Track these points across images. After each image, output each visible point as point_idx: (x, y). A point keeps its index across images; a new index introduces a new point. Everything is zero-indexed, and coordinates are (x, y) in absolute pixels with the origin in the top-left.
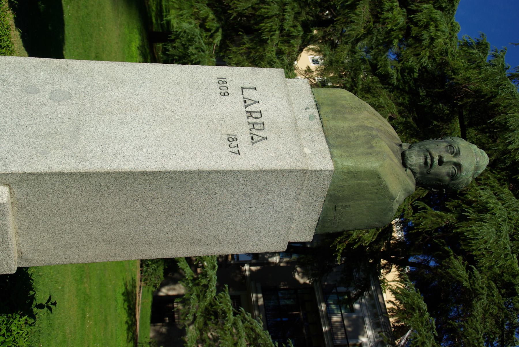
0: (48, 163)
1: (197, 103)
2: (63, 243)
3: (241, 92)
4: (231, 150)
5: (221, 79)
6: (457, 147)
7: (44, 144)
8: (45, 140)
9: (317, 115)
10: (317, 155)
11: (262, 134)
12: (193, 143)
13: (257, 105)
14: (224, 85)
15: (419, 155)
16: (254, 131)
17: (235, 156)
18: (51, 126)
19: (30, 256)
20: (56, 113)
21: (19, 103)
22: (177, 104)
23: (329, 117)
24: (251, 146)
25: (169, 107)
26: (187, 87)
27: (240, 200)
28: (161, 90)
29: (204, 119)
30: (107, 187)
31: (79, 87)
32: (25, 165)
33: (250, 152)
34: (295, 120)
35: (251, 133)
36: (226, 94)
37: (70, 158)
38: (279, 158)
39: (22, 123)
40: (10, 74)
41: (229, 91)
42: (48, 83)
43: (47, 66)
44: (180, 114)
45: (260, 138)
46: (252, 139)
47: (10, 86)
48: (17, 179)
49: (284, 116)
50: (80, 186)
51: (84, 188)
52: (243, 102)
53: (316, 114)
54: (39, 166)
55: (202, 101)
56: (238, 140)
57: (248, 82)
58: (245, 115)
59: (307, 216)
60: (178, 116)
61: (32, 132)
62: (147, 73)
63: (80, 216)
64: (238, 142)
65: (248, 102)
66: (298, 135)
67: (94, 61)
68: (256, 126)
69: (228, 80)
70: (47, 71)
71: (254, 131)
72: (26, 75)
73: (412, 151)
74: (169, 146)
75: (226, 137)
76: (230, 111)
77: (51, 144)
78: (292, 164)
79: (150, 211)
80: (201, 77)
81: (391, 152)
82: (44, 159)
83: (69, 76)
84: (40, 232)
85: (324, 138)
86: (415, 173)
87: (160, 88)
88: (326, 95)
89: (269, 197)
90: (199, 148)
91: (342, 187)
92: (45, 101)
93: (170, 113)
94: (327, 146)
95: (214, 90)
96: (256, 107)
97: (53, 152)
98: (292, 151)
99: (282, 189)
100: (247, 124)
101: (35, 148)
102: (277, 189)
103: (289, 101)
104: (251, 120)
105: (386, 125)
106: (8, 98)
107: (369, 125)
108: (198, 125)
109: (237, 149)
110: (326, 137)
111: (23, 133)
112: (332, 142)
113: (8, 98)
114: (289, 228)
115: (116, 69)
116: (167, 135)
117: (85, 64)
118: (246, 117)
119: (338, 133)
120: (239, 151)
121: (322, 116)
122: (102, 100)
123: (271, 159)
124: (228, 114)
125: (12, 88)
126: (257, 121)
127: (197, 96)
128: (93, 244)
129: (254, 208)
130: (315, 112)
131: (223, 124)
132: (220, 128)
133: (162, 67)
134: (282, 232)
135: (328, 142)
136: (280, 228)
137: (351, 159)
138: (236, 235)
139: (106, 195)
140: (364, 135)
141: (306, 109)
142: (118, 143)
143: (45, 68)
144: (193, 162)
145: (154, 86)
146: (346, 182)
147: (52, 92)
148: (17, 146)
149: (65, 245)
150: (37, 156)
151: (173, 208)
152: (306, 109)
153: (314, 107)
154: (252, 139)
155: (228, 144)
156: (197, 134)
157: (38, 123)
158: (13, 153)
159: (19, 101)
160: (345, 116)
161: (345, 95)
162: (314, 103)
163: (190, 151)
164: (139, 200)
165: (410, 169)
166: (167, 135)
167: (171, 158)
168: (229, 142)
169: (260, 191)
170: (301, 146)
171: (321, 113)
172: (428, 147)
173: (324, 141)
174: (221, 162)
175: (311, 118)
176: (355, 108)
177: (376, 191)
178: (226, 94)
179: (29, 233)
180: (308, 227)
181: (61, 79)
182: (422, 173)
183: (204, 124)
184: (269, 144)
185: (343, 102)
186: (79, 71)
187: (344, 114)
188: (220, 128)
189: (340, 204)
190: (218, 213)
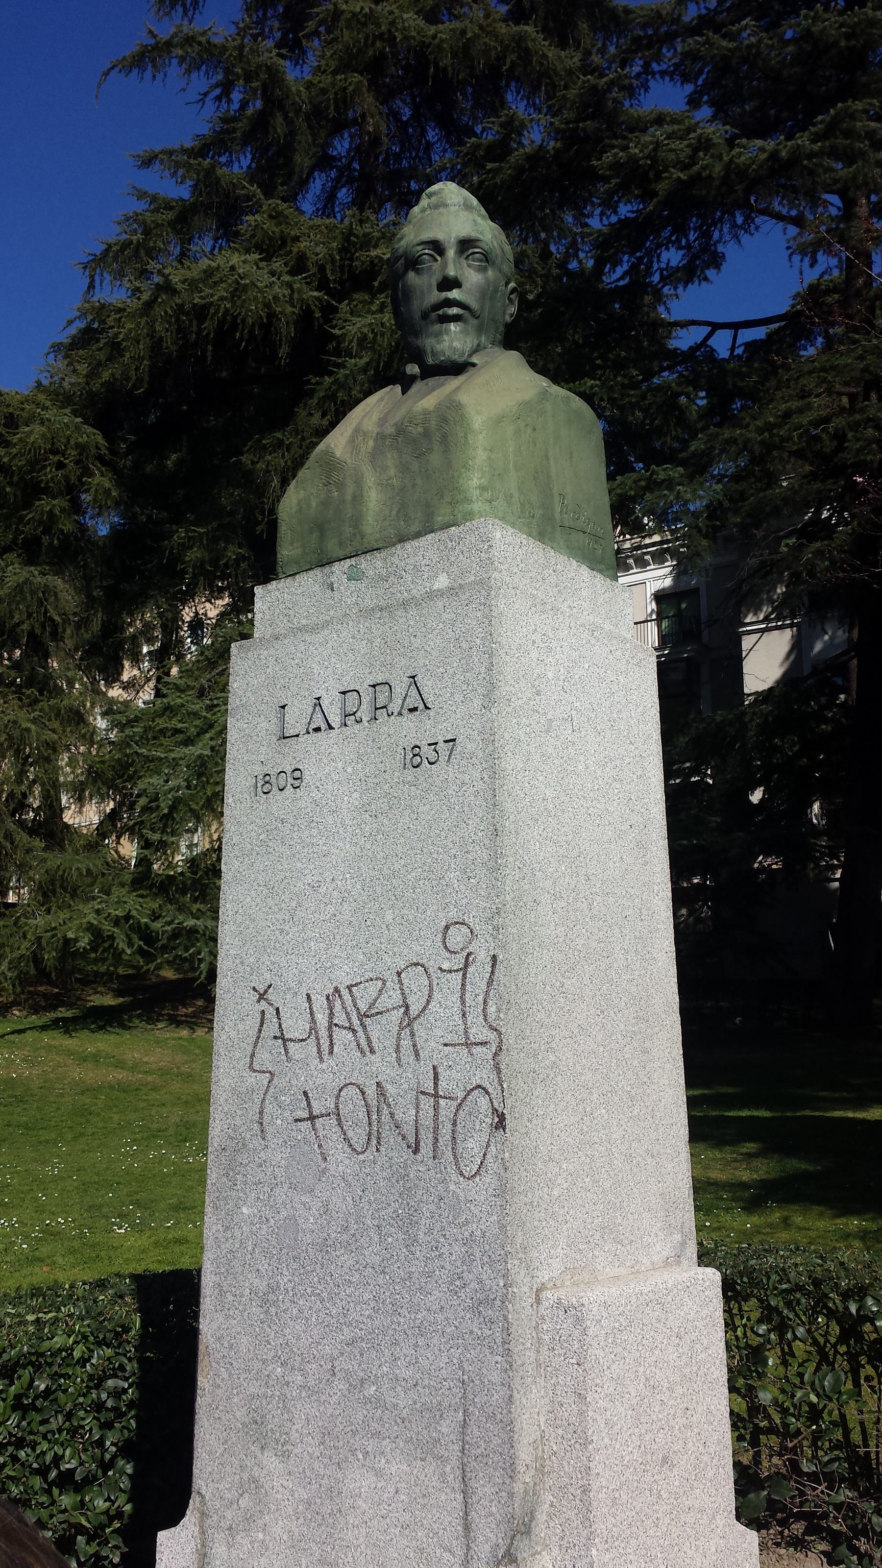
0: (482, 1198)
1: (321, 842)
2: (649, 1160)
3: (293, 741)
4: (443, 758)
5: (259, 789)
6: (419, 248)
7: (432, 1207)
8: (422, 1205)
9: (348, 562)
10: (453, 559)
11: (399, 690)
12: (425, 850)
13: (325, 703)
14: (273, 780)
15: (438, 335)
16: (395, 707)
17: (459, 748)
18: (384, 1191)
19: (678, 1237)
20: (350, 1178)
21: (322, 1265)
22: (323, 890)
23: (354, 535)
24: (432, 713)
25: (331, 909)
26: (280, 868)
27: (558, 743)
28: (287, 928)
29: (363, 826)
30: (535, 1056)
31: (279, 1122)
32: (490, 1253)
33: (449, 713)
34: (367, 613)
35: (400, 714)
36: (297, 774)
37: (470, 1145)
38: (464, 645)
39: (377, 1260)
40: (247, 1284)
41: (289, 769)
42: (269, 1196)
43: (225, 1198)
44: (348, 882)
45: (413, 691)
46: (414, 710)
47: (278, 1287)
48: (522, 1273)
49: (353, 637)
50: (534, 1122)
51: (540, 1112)
52: (319, 734)
53: (346, 566)
54: (492, 1219)
55: (315, 832)
56: (418, 743)
57: (264, 725)
58: (354, 728)
59: (584, 593)
60: (354, 887)
61: (401, 1236)
62: (242, 963)
63: (596, 1121)
64: (423, 744)
65: (319, 721)
66: (404, 605)
67: (213, 1087)
68: (381, 701)
69: (259, 770)
70: (239, 1198)
71: (395, 707)
72: (250, 1248)
73: (429, 350)
74: (435, 907)
75: (410, 773)
76: (340, 765)
77: (433, 1190)
78: (479, 614)
79: (582, 955)
80: (253, 834)
81: (435, 393)
82: (473, 1208)
83: (251, 1146)
84: (629, 1215)
85: (408, 545)
86: (478, 345)
87: (282, 931)
88: (295, 545)
89: (550, 675)
90: (439, 836)
91: (523, 505)
92: (316, 1204)
93: (346, 906)
94: (429, 537)
95: (287, 802)
96: (331, 704)
97: (452, 1187)
98: (445, 616)
99: (534, 642)
100: (375, 725)
101: (443, 1228)
102: (534, 655)
103: (314, 629)
104: (364, 713)
105: (382, 399)
106: (309, 1290)
107: (371, 443)
108: (378, 837)
109: (441, 746)
110: (402, 539)
111: (402, 1257)
112: (415, 528)
113: (309, 1290)
114: (611, 636)
115: (233, 1034)
116: (405, 911)
117: (220, 1108)
118: (358, 726)
119: (394, 513)
120: (445, 742)
121: (349, 550)
122: (313, 1068)
123: (468, 664)
124: (349, 770)
125: (283, 1281)
126: (366, 699)
127: (303, 842)
128: (649, 1091)
129: (574, 713)
130: (339, 569)
131: (375, 781)
132: (386, 787)
133: (226, 927)
134: (619, 653)
135: (418, 535)
136: (610, 657)
137: (461, 481)
138: (628, 760)
139: (552, 1058)
140: (396, 455)
141: (333, 590)
142: (426, 1029)
143: (231, 1205)
144: (477, 848)
145: (278, 945)
146: (512, 496)
147: (293, 1187)
148: (437, 1272)
149: (652, 1156)
150: (464, 1225)
151: (576, 900)
152: (333, 590)
153: (327, 569)
154: (414, 710)
155: (429, 766)
156: (402, 840)
157: (376, 1223)
158: (458, 1283)
159: (318, 1266)
160: (349, 498)
161: (294, 502)
162: (317, 572)
163: (446, 858)
164: (562, 980)
165: (470, 355)
166: (405, 911)
167: (465, 901)
168: (423, 765)
169: (538, 693)
170: (432, 595)
171: (341, 554)
172: (417, 315)
173: (415, 543)
174: (475, 783)
175: (354, 576)
176: (329, 477)
177: (529, 430)
178: (297, 774)
179: (632, 1241)
180: (606, 595)
181: (260, 1165)
182: (480, 330)
183: (375, 825)
184: (428, 670)
185: (314, 504)
186: (238, 1122)
187: (344, 501)
188: (386, 787)
189: (557, 516)
190: (584, 797)
